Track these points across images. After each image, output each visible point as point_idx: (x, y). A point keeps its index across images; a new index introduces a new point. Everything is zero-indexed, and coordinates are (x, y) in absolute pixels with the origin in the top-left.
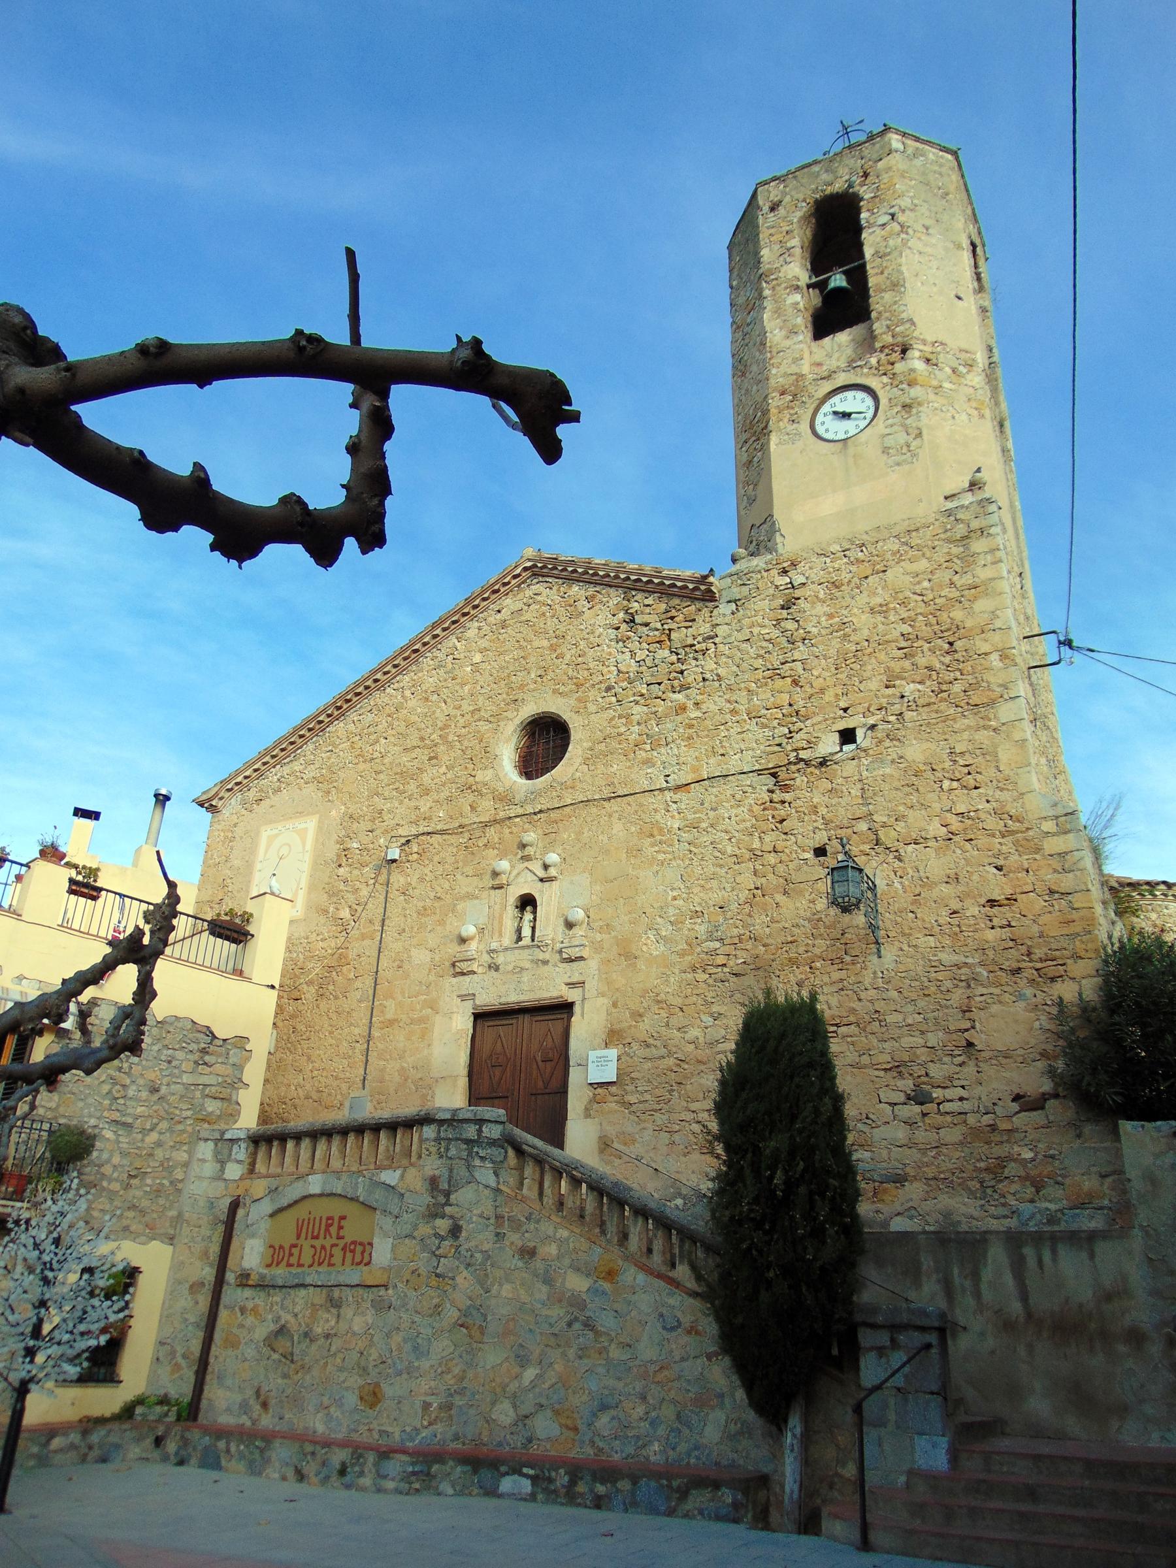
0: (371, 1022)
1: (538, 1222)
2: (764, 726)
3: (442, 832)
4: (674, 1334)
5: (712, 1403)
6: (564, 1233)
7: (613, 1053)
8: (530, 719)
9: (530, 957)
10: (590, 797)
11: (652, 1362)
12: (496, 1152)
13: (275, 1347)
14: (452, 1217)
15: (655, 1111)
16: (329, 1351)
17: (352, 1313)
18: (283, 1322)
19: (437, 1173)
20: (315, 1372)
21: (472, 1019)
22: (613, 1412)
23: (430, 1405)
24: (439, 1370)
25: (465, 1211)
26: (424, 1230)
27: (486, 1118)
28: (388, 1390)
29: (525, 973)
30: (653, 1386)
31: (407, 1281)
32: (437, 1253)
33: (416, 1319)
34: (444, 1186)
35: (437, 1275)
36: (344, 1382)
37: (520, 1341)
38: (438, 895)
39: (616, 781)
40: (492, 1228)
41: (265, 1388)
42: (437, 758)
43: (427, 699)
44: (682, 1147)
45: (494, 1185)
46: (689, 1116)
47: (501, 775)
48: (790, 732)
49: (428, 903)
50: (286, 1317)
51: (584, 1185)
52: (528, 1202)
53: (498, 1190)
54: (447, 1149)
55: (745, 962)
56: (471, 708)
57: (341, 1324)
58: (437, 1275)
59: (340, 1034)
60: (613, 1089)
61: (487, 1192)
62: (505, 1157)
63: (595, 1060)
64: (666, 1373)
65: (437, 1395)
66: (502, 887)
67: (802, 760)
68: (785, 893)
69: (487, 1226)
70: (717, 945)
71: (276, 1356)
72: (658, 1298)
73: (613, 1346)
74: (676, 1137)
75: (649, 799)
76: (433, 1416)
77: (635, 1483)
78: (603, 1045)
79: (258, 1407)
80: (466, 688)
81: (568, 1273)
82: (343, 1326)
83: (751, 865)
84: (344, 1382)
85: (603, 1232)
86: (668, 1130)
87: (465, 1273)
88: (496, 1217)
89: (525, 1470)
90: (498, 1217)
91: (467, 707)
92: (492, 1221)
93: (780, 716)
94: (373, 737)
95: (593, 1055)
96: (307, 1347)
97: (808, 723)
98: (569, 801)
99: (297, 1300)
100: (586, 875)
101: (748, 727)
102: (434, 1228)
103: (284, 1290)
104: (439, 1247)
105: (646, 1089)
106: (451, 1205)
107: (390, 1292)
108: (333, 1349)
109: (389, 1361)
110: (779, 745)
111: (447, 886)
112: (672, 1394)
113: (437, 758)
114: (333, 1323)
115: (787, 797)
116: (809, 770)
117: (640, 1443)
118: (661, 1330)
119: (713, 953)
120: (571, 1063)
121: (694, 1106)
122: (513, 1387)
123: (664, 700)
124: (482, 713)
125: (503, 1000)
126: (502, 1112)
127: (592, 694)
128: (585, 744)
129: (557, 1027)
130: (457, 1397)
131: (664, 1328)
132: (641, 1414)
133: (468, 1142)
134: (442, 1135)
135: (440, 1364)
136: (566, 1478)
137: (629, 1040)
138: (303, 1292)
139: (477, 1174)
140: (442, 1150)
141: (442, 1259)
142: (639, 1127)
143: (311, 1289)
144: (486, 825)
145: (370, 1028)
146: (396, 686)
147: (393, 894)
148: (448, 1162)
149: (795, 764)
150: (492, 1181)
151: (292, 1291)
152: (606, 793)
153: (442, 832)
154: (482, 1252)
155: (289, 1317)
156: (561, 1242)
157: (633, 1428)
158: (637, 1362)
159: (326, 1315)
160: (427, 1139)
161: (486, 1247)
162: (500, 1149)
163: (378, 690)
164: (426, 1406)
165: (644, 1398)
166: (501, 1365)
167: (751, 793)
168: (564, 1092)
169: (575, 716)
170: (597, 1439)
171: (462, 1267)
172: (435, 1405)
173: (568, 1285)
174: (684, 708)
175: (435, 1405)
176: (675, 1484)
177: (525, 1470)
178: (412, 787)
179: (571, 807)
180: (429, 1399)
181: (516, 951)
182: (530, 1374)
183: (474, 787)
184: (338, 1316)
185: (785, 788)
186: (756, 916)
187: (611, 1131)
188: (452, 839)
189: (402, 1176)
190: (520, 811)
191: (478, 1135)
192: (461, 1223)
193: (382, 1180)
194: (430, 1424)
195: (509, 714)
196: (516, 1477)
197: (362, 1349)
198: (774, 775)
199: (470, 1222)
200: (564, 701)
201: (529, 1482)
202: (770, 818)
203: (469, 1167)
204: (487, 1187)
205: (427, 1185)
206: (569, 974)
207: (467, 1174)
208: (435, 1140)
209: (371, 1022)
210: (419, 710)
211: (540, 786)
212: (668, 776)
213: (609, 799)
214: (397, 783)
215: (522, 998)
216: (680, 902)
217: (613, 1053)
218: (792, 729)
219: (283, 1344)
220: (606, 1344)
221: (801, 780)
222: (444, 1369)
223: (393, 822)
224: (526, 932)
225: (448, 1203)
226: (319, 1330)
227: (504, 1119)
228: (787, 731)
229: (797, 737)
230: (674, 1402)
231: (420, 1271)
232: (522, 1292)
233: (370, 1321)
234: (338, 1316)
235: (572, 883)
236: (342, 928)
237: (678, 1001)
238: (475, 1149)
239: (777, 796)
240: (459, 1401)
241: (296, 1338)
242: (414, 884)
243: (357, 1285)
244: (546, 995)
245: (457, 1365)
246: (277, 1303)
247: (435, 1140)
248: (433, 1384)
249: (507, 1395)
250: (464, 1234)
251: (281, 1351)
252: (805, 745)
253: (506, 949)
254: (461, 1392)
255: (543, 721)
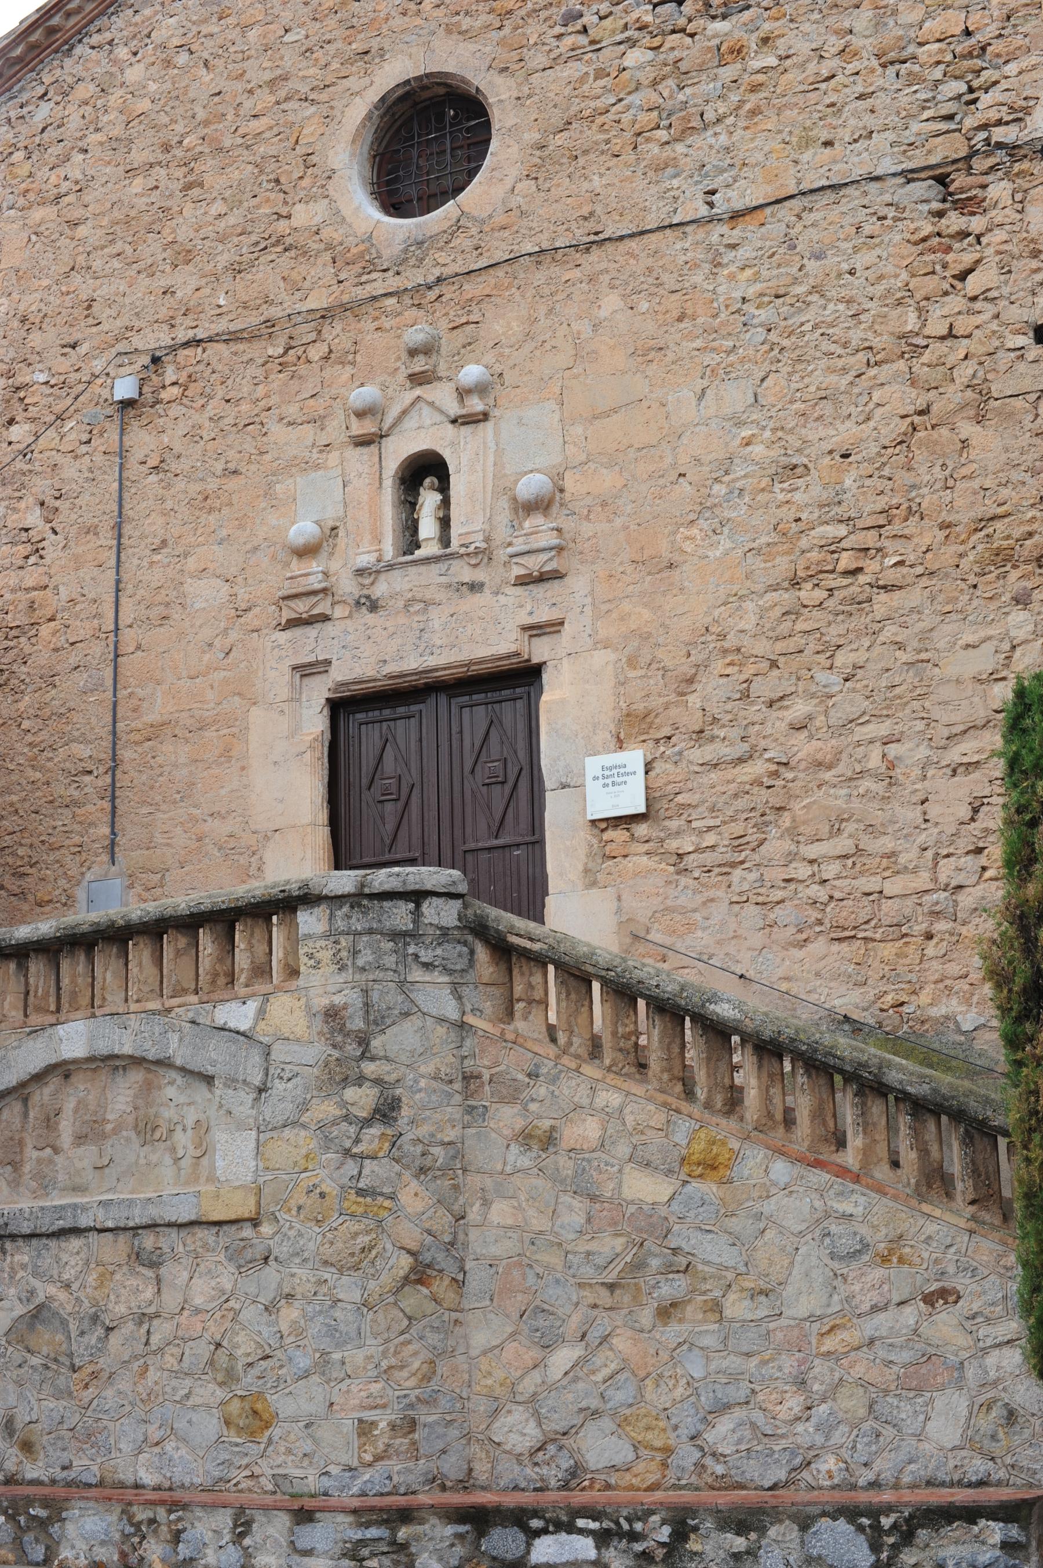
0: (114, 733)
1: (554, 1080)
2: (913, 79)
3: (232, 338)
4: (854, 1265)
5: (939, 1379)
6: (614, 1099)
7: (634, 758)
8: (400, 92)
9: (443, 579)
10: (545, 245)
11: (812, 1318)
12: (452, 952)
13: (32, 1344)
14: (378, 1081)
15: (733, 865)
16: (147, 1343)
17: (185, 1275)
18: (40, 1298)
19: (338, 1000)
20: (124, 1384)
21: (326, 712)
22: (739, 1413)
23: (373, 1424)
24: (384, 1364)
25: (403, 1069)
26: (326, 1109)
27: (428, 887)
28: (282, 1404)
29: (434, 612)
30: (817, 1362)
31: (299, 1208)
32: (355, 1150)
33: (327, 1276)
34: (357, 1023)
35: (361, 1192)
36: (187, 1396)
37: (538, 1302)
38: (232, 466)
39: (599, 209)
40: (458, 1098)
41: (22, 1418)
42: (201, 185)
43: (168, 63)
44: (793, 930)
45: (453, 1015)
46: (803, 871)
47: (346, 212)
48: (971, 90)
49: (212, 484)
50: (45, 1290)
51: (641, 1003)
52: (529, 1045)
53: (462, 1026)
54: (355, 953)
55: (901, 563)
56: (268, 76)
57: (165, 1296)
58: (361, 1192)
59: (50, 759)
60: (642, 830)
61: (441, 1030)
62: (472, 962)
63: (599, 773)
64: (843, 1335)
65: (384, 1406)
66: (373, 442)
67: (1000, 145)
68: (980, 419)
69: (450, 1096)
70: (842, 530)
71: (35, 1361)
72: (818, 1204)
73: (732, 1297)
74: (778, 913)
75: (672, 245)
76: (381, 1447)
77: (804, 1527)
78: (613, 744)
79: (15, 1450)
80: (252, 35)
81: (627, 1169)
82: (171, 1300)
83: (901, 365)
84: (187, 1396)
85: (689, 1094)
86: (760, 899)
87: (414, 1184)
88: (464, 1078)
89: (581, 1523)
90: (467, 1078)
91: (258, 72)
92: (458, 1086)
93: (949, 57)
94: (56, 150)
95: (593, 765)
96: (99, 1339)
97: (1012, 68)
98: (500, 256)
99: (65, 1257)
100: (552, 405)
101: (881, 82)
102: (344, 1104)
103: (34, 1242)
104: (357, 1141)
105: (711, 823)
106: (373, 1059)
107: (266, 1229)
108: (155, 1339)
109: (278, 1353)
110: (950, 117)
111: (249, 447)
112: (859, 1371)
113: (201, 185)
114: (149, 1293)
115: (977, 224)
116: (1017, 167)
117: (798, 1461)
118: (829, 1262)
119: (834, 547)
120: (548, 784)
121: (812, 851)
122: (528, 1385)
123: (692, 35)
124: (292, 84)
125: (388, 669)
126: (456, 873)
127: (533, 31)
128: (526, 136)
129: (510, 713)
130: (423, 1409)
131: (832, 1256)
132: (797, 1409)
133: (395, 935)
134: (340, 924)
135: (384, 1354)
136: (666, 1530)
137: (666, 731)
138: (75, 1243)
139: (419, 998)
140: (344, 954)
141: (367, 1162)
142: (699, 899)
143: (93, 1237)
144: (326, 315)
145: (114, 744)
146: (96, 39)
147: (134, 469)
148: (357, 977)
149: (988, 154)
150: (451, 1010)
151: (53, 1243)
152: (580, 234)
153: (232, 338)
154: (443, 1144)
155: (52, 1290)
156: (607, 1115)
157: (783, 1436)
158: (783, 1322)
159: (133, 1282)
160: (309, 936)
161: (451, 1134)
162: (459, 947)
163: (56, 51)
164: (365, 1428)
165: (801, 1383)
166: (501, 1347)
167: (896, 219)
168: (537, 844)
169: (499, 80)
170: (708, 1461)
171: (407, 1175)
172: (382, 1425)
173: (627, 1193)
174: (738, 51)
175: (382, 1425)
176: (886, 1522)
177: (581, 1523)
178: (152, 249)
179: (506, 267)
180: (368, 1415)
181: (413, 570)
182: (563, 1358)
183: (289, 240)
184: (158, 1280)
185: (968, 205)
186: (923, 469)
187: (641, 909)
188: (256, 351)
189: (261, 1013)
190: (393, 283)
191: (414, 922)
192: (398, 1092)
193: (220, 1022)
194: (378, 1458)
195: (353, 83)
196: (563, 1536)
197: (218, 1337)
198: (942, 180)
199: (414, 1090)
200: (472, 47)
201: (589, 1542)
202: (938, 267)
203: (403, 985)
204: (441, 1020)
205: (319, 1023)
206: (529, 608)
207: (400, 998)
208: (326, 936)
209: (114, 733)
210: (153, 87)
211: (436, 230)
212: (713, 192)
213: (588, 247)
214: (120, 243)
215: (432, 662)
216: (758, 450)
217: (634, 758)
218: (975, 84)
219: (47, 1339)
220: (717, 1293)
221: (999, 190)
222: (393, 1361)
223: (119, 323)
224: (428, 528)
225: (366, 1055)
226: (121, 1309)
227: (463, 888)
228: (964, 88)
229: (986, 99)
230: (864, 1384)
231: (324, 1188)
232: (531, 1212)
233: (228, 1287)
234: (158, 1280)
235: (520, 423)
236: (29, 548)
237: (762, 647)
238: (411, 950)
239: (954, 221)
240: (427, 1417)
241: (73, 1327)
242: (178, 448)
243: (192, 1223)
244: (482, 652)
245: (415, 1354)
246: (24, 1267)
247: (326, 936)
248: (375, 1388)
249: (519, 1398)
250: (406, 1112)
251: (45, 1350)
252: (1004, 114)
253: (391, 567)
254: (429, 1402)
255: (426, 94)
